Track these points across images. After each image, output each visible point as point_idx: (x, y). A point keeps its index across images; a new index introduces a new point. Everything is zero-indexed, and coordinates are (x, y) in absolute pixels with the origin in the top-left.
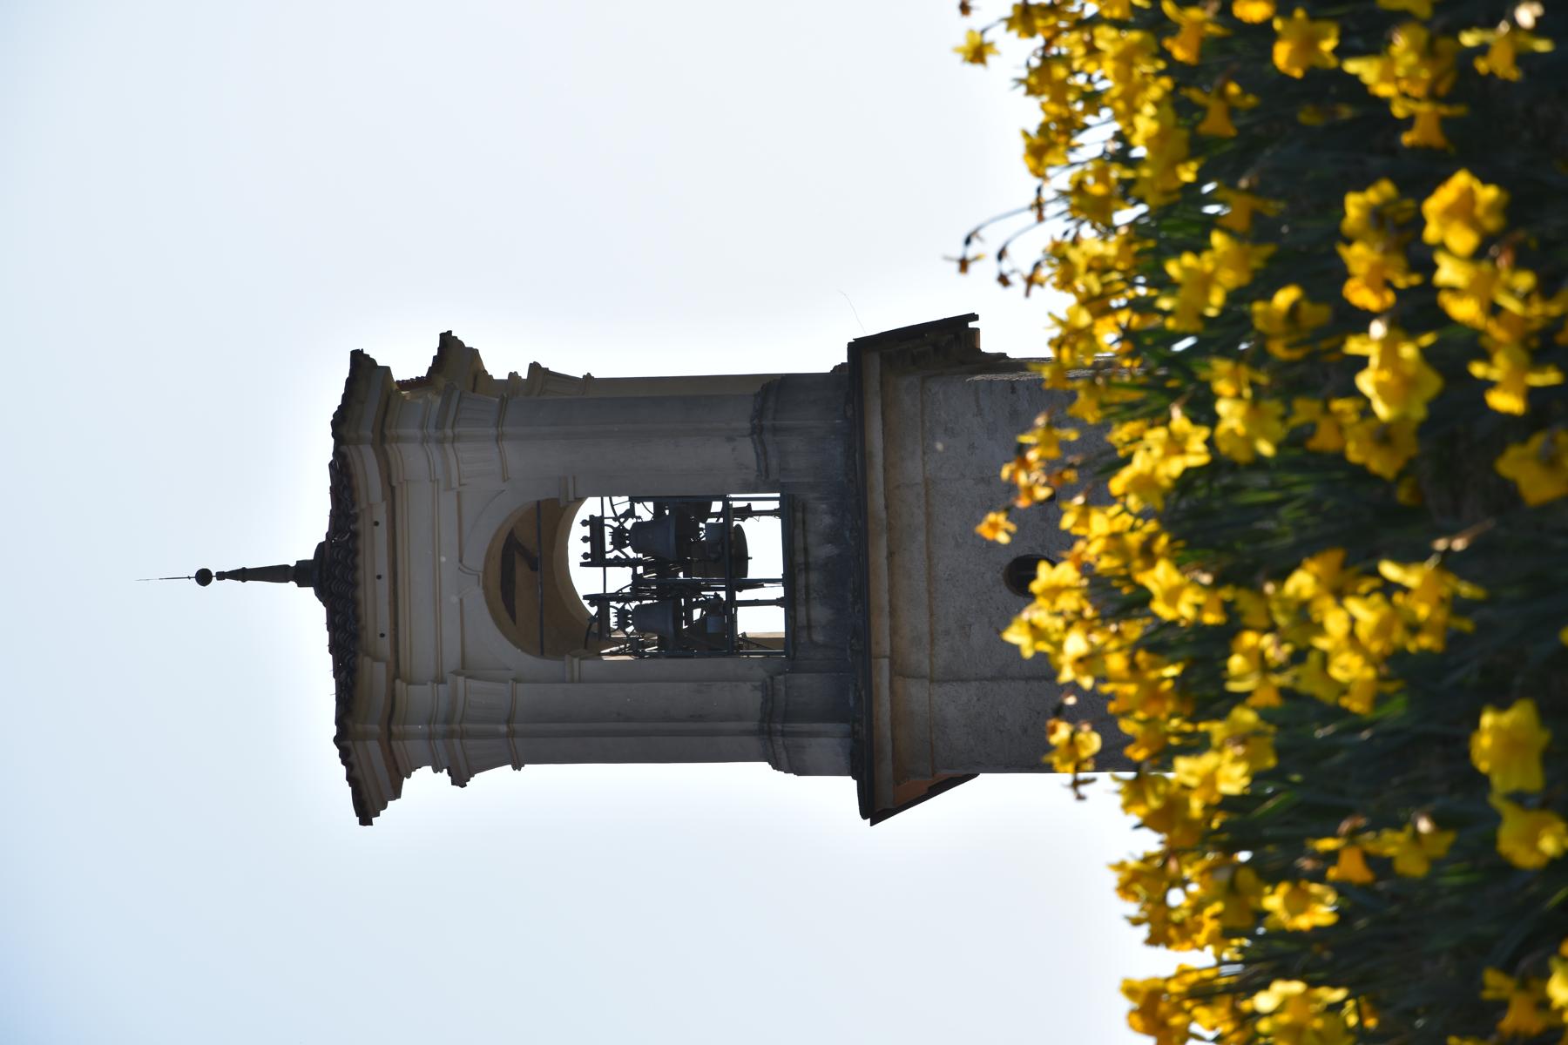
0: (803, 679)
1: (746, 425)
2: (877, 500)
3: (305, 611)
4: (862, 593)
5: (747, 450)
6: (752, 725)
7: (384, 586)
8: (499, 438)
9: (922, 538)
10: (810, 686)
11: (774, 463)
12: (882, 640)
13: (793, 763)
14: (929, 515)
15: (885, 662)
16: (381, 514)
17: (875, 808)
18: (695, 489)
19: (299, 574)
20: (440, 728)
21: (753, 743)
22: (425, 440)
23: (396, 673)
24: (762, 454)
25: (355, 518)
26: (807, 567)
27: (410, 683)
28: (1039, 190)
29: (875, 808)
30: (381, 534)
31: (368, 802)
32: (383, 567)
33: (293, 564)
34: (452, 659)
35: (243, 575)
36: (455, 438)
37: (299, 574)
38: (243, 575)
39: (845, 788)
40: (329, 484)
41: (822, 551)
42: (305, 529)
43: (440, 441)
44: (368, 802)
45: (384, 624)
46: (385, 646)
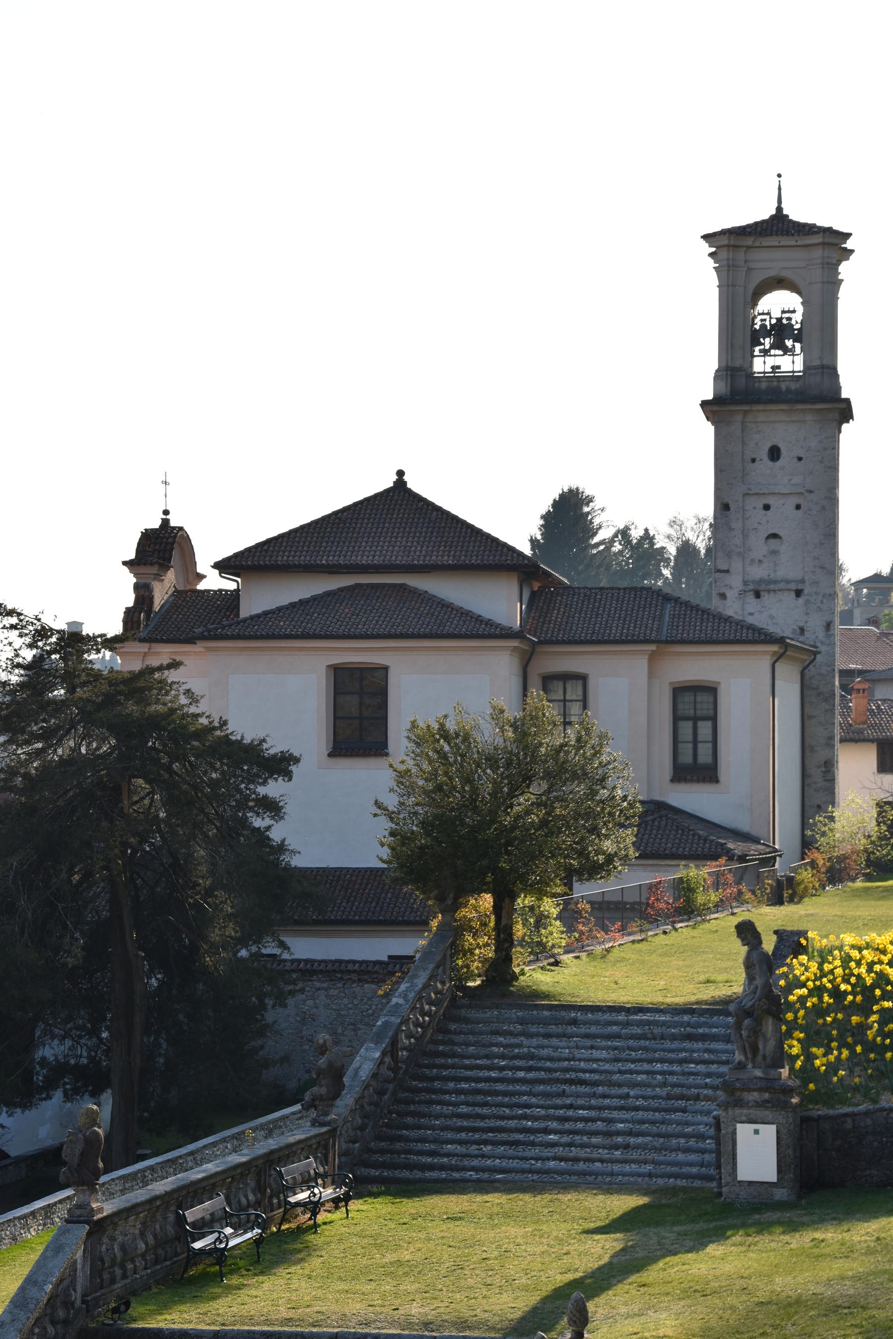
0: (743, 380)
1: (825, 363)
2: (800, 406)
3: (766, 212)
4: (770, 402)
5: (817, 363)
6: (730, 364)
7: (777, 244)
8: (823, 282)
9: (787, 419)
10: (741, 383)
11: (812, 371)
12: (756, 407)
13: (719, 376)
14: (794, 422)
15: (748, 408)
16: (799, 243)
17: (704, 404)
18: (804, 339)
19: (779, 209)
20: (731, 262)
21: (724, 364)
22: (823, 258)
23: (748, 247)
24: (815, 368)
25: (799, 235)
26: (778, 381)
27: (745, 252)
28: (391, 766)
29: (704, 404)
30: (793, 243)
31: (706, 237)
32: (782, 244)
33: (785, 212)
34: (752, 265)
35: (780, 189)
36: (823, 268)
37: (779, 209)
38: (780, 189)
39: (710, 396)
40: (841, 380)
41: (783, 386)
42: (796, 213)
43: (823, 264)
44: (706, 237)
45: (764, 244)
46: (757, 244)
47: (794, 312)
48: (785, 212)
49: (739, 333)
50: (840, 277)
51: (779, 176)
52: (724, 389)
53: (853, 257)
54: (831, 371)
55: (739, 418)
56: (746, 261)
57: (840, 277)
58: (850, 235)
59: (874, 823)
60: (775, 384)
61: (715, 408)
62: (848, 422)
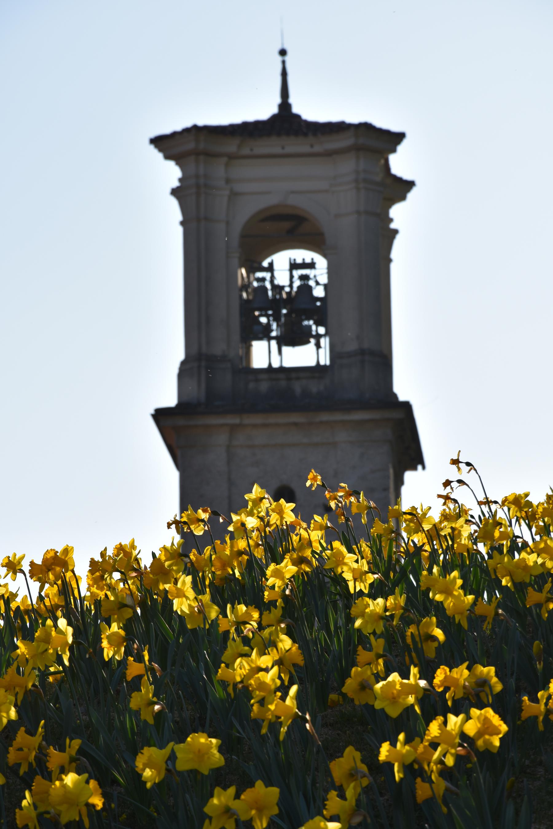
2: (325, 417)
3: (265, 109)
4: (275, 409)
5: (352, 346)
7: (277, 150)
8: (358, 212)
16: (317, 149)
19: (285, 106)
23: (231, 157)
24: (350, 355)
29: (160, 416)
34: (239, 187)
35: (284, 74)
37: (285, 106)
38: (284, 74)
39: (170, 399)
41: (297, 387)
42: (311, 108)
43: (356, 181)
46: (246, 151)
47: (312, 265)
48: (295, 110)
49: (220, 310)
50: (393, 226)
51: (283, 53)
52: (196, 392)
53: (411, 196)
54: (379, 359)
55: (221, 439)
56: (228, 181)
57: (393, 226)
58: (399, 137)
59: (291, 575)
60: (283, 383)
61: (180, 421)
62: (415, 468)
